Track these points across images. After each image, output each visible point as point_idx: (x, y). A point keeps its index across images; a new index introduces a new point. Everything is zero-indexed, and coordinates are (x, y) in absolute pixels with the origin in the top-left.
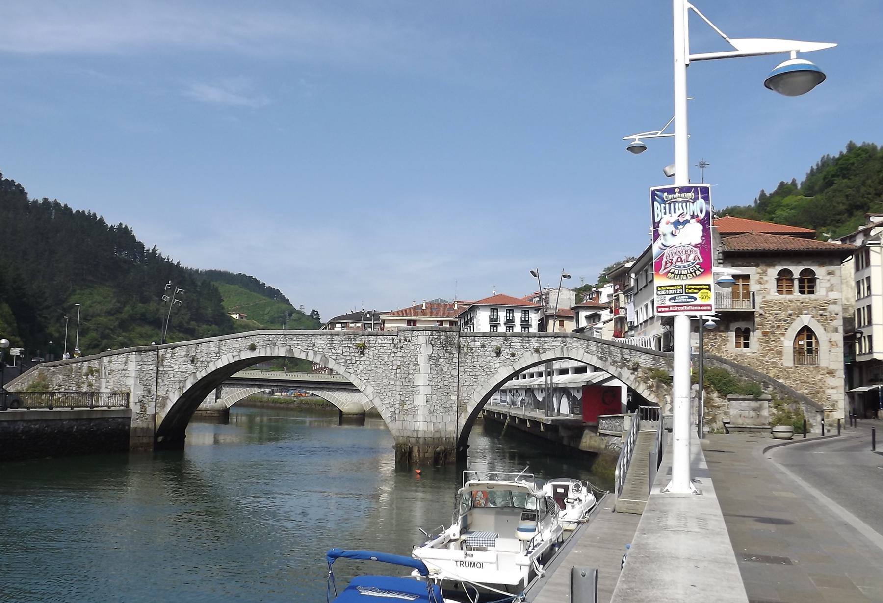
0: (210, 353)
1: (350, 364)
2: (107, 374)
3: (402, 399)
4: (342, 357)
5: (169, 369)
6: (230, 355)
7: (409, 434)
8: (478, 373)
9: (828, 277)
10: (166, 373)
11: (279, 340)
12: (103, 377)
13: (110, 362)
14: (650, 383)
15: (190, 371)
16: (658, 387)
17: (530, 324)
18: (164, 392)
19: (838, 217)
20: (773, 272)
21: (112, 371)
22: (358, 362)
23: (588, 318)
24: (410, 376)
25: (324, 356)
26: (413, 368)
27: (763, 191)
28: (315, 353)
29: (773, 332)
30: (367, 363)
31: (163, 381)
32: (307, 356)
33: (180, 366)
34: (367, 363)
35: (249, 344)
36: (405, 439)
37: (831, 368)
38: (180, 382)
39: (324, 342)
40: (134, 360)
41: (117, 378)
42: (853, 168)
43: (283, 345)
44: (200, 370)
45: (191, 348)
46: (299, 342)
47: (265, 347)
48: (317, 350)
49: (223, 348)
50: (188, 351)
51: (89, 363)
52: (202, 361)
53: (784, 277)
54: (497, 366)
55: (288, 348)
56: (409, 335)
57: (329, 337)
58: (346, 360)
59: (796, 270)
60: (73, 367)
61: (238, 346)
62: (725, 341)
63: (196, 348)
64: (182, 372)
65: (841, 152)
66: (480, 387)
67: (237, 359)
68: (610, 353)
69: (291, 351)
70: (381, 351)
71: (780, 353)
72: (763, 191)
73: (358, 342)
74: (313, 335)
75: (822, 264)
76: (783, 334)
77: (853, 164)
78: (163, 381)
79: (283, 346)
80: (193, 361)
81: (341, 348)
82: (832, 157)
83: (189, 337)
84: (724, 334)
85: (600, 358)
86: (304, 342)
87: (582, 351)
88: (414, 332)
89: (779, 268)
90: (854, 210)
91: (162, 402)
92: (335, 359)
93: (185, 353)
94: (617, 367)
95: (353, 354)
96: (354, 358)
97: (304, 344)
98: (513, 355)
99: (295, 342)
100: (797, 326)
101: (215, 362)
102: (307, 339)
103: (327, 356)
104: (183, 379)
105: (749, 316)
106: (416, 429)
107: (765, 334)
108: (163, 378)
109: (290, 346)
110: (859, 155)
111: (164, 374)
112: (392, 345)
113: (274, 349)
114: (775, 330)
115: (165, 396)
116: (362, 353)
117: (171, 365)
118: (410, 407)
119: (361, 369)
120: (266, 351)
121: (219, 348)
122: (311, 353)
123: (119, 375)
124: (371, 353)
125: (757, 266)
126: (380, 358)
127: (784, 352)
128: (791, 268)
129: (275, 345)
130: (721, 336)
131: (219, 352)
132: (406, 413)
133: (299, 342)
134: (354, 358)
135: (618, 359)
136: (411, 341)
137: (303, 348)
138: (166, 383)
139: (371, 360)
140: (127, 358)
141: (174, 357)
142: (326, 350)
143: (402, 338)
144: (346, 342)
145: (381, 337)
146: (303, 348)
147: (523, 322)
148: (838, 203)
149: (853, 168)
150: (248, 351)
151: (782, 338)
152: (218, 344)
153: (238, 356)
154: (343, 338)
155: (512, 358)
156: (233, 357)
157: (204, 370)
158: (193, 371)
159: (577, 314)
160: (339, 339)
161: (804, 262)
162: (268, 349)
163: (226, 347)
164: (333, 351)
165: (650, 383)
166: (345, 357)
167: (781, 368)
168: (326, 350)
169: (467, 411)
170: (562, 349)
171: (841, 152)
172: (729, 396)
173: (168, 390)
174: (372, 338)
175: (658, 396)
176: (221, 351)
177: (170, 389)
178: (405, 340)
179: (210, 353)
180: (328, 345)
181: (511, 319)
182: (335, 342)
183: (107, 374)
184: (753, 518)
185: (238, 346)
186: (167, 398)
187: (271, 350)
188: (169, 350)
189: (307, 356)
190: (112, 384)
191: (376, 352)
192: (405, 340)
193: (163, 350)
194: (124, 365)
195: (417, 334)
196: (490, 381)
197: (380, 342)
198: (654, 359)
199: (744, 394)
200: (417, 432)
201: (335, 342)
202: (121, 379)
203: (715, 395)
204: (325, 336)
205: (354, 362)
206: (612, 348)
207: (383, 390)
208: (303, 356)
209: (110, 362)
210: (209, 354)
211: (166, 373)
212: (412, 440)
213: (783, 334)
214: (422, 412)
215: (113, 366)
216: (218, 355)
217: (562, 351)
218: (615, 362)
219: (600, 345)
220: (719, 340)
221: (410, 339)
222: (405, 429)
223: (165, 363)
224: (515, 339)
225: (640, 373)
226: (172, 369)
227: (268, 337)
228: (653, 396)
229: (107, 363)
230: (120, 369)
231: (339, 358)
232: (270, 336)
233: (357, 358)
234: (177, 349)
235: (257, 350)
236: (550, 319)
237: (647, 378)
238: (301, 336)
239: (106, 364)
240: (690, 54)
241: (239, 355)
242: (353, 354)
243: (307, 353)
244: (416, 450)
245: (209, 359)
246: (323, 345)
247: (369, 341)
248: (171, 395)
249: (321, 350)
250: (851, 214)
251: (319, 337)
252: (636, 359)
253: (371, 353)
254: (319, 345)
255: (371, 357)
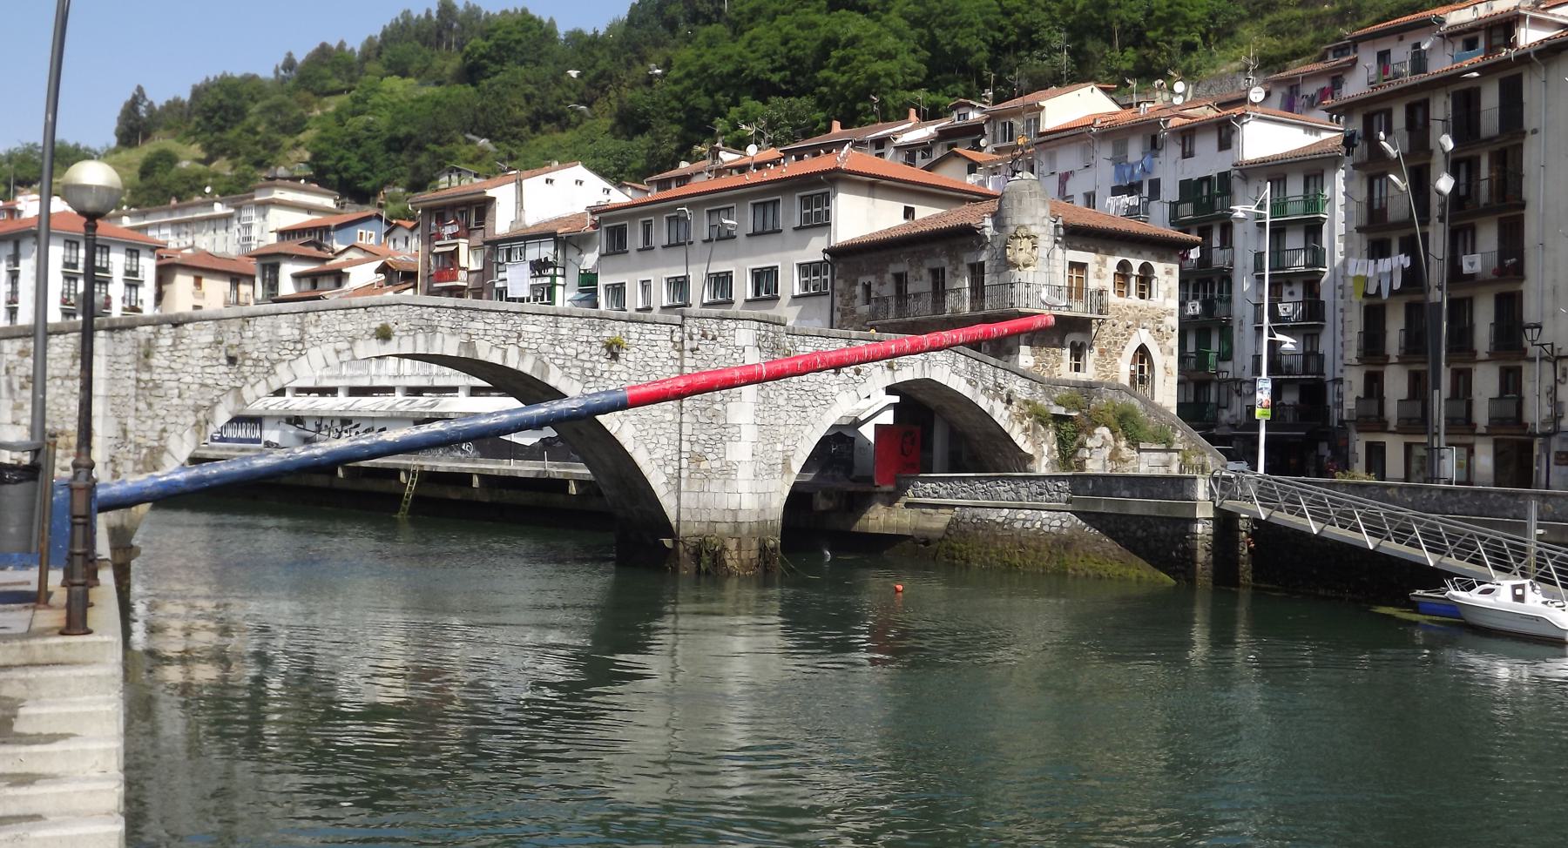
0: (280, 342)
1: (592, 379)
3: (697, 449)
4: (576, 362)
5: (166, 377)
7: (715, 516)
8: (807, 403)
10: (157, 387)
11: (445, 320)
14: (1026, 423)
15: (225, 382)
16: (1035, 429)
17: (140, 278)
18: (155, 435)
19: (515, 130)
20: (1113, 262)
22: (606, 375)
23: (297, 277)
24: (717, 406)
25: (540, 359)
27: (290, 54)
28: (522, 352)
31: (150, 405)
32: (504, 357)
33: (198, 370)
35: (377, 325)
36: (704, 526)
38: (197, 409)
39: (539, 329)
42: (519, 48)
43: (454, 331)
44: (252, 380)
45: (229, 326)
46: (488, 327)
47: (413, 331)
48: (525, 345)
49: (312, 330)
50: (219, 333)
52: (258, 360)
53: (1123, 270)
54: (835, 390)
55: (465, 338)
56: (714, 326)
57: (551, 318)
58: (583, 370)
59: (1136, 263)
61: (349, 327)
62: (1059, 360)
63: (242, 327)
64: (203, 385)
65: (596, 32)
69: (470, 345)
72: (290, 54)
73: (607, 333)
74: (516, 313)
75: (1161, 259)
77: (519, 42)
78: (150, 405)
79: (454, 334)
80: (232, 360)
82: (415, 17)
84: (1057, 350)
85: (969, 382)
86: (499, 326)
87: (947, 370)
88: (725, 322)
89: (1119, 259)
90: (542, 123)
91: (149, 459)
92: (562, 367)
93: (211, 338)
95: (596, 358)
96: (599, 366)
97: (499, 333)
99: (481, 325)
100: (1133, 346)
101: (292, 364)
102: (504, 321)
103: (546, 359)
104: (207, 403)
105: (1082, 325)
106: (733, 506)
107: (1102, 352)
108: (152, 400)
109: (470, 335)
110: (529, 29)
111: (152, 389)
112: (671, 344)
113: (433, 340)
114: (1112, 347)
115: (156, 444)
116: (615, 357)
117: (173, 365)
118: (717, 464)
120: (415, 342)
121: (302, 330)
122: (513, 353)
125: (1096, 252)
126: (648, 369)
128: (1130, 260)
129: (434, 330)
130: (1054, 353)
131: (301, 341)
132: (707, 476)
133: (488, 327)
134: (599, 366)
135: (990, 384)
136: (719, 339)
138: (159, 412)
139: (631, 371)
141: (181, 347)
142: (545, 347)
143: (695, 330)
144: (585, 333)
145: (649, 326)
146: (496, 341)
147: (128, 273)
148: (514, 106)
149: (519, 48)
150: (374, 341)
152: (298, 320)
153: (349, 352)
154: (578, 323)
155: (856, 377)
157: (263, 382)
158: (232, 384)
159: (275, 268)
160: (570, 325)
161: (1144, 253)
162: (421, 338)
163: (320, 330)
164: (558, 349)
165: (1026, 423)
166: (581, 364)
168: (545, 347)
171: (596, 32)
172: (1142, 446)
173: (164, 430)
174: (633, 328)
175: (1034, 444)
176: (307, 337)
177: (170, 428)
178: (704, 335)
179: (280, 342)
180: (549, 337)
181: (104, 265)
182: (563, 331)
183: (16, 386)
185: (349, 327)
186: (163, 450)
187: (426, 341)
188: (166, 329)
189: (504, 357)
192: (704, 335)
193: (149, 329)
197: (648, 337)
199: (1156, 442)
200: (735, 512)
201: (563, 331)
202: (62, 401)
203: (1123, 443)
204: (541, 318)
205: (598, 373)
206: (984, 367)
207: (652, 432)
210: (275, 342)
211: (157, 387)
212: (723, 528)
214: (744, 474)
216: (299, 346)
218: (987, 389)
219: (970, 360)
220: (1051, 358)
221: (717, 333)
222: (705, 508)
223: (154, 361)
225: (1014, 408)
226: (174, 377)
227: (418, 311)
228: (1028, 443)
229: (16, 357)
231: (568, 364)
232: (424, 309)
233: (605, 367)
234: (189, 326)
235: (395, 340)
236: (178, 270)
237: (1023, 415)
238: (493, 315)
239: (10, 358)
241: (351, 349)
242: (596, 358)
243: (505, 351)
244: (732, 545)
245: (276, 356)
246: (538, 336)
248: (173, 442)
249: (535, 346)
250: (536, 128)
251: (530, 318)
252: (1011, 386)
253: (631, 357)
254: (530, 335)
255: (630, 365)
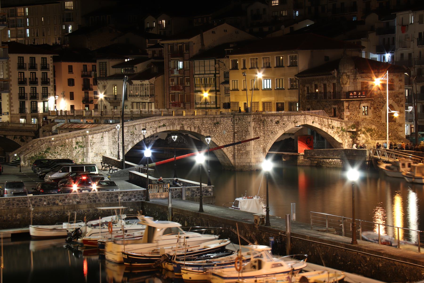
2: (92, 144)
6: (151, 131)
8: (270, 134)
9: (400, 82)
12: (90, 146)
13: (93, 138)
21: (94, 143)
22: (215, 131)
26: (245, 133)
28: (195, 128)
29: (378, 108)
30: (220, 131)
32: (191, 129)
34: (220, 131)
37: (401, 123)
40: (107, 136)
41: (97, 146)
48: (195, 126)
49: (148, 127)
51: (76, 139)
54: (278, 130)
55: (181, 125)
58: (210, 130)
60: (67, 142)
66: (271, 140)
67: (155, 132)
68: (323, 121)
69: (183, 127)
70: (226, 125)
71: (380, 117)
76: (382, 108)
81: (207, 125)
83: (283, 139)
85: (319, 124)
92: (204, 130)
94: (326, 128)
96: (213, 129)
98: (284, 124)
103: (201, 129)
114: (379, 106)
119: (217, 134)
120: (170, 127)
123: (98, 145)
124: (221, 126)
127: (382, 117)
134: (213, 129)
135: (327, 124)
137: (188, 126)
140: (103, 135)
142: (200, 126)
143: (237, 118)
146: (188, 126)
151: (381, 111)
155: (284, 126)
156: (153, 131)
164: (204, 126)
167: (381, 123)
168: (200, 126)
169: (266, 152)
170: (304, 121)
184: (195, 252)
187: (173, 127)
189: (191, 129)
190: (95, 149)
191: (224, 126)
194: (101, 139)
195: (247, 117)
196: (275, 137)
198: (340, 123)
208: (189, 129)
209: (93, 138)
213: (382, 108)
215: (94, 140)
217: (304, 122)
218: (325, 125)
224: (285, 117)
230: (99, 141)
233: (215, 129)
240: (163, 62)
247: (220, 120)
253: (221, 126)
